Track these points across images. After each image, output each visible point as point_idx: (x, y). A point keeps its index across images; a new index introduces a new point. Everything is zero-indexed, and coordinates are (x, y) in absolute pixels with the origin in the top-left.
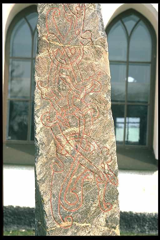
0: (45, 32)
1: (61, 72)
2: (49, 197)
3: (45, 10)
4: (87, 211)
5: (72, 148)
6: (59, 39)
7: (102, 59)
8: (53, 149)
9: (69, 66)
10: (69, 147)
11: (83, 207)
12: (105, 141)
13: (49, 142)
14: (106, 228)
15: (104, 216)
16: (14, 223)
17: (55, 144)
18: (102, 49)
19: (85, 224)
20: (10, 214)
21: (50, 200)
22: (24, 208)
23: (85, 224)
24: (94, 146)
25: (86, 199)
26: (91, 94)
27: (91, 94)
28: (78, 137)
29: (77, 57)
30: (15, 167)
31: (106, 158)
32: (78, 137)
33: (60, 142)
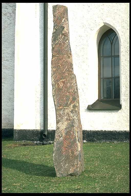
0: (54, 52)
1: (58, 64)
2: (56, 100)
3: (54, 46)
4: (67, 103)
5: (62, 86)
6: (58, 54)
7: (70, 59)
8: (57, 86)
9: (61, 62)
10: (61, 85)
11: (66, 102)
12: (72, 83)
13: (56, 84)
14: (73, 108)
15: (72, 105)
16: (103, 139)
17: (58, 85)
18: (70, 56)
19: (67, 107)
20: (101, 134)
21: (56, 101)
22: (108, 131)
23: (67, 107)
24: (69, 85)
25: (67, 100)
26: (67, 69)
27: (67, 69)
28: (64, 82)
29: (63, 59)
30: (105, 111)
31: (72, 88)
32: (64, 82)
33: (58, 84)
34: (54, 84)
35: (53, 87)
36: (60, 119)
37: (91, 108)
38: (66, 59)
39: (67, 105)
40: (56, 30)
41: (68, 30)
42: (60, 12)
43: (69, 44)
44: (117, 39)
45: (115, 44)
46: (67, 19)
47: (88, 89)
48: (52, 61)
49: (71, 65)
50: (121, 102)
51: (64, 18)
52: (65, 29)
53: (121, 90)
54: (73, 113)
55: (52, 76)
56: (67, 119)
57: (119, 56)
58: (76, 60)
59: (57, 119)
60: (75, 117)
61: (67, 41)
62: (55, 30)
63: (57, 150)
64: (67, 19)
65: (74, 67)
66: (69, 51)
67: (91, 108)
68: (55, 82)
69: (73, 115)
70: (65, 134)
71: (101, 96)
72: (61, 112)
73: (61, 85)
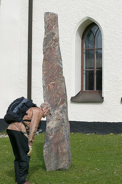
4: (57, 104)
12: (61, 86)
24: (59, 87)
32: (54, 85)
34: (45, 86)
36: (50, 118)
37: (74, 100)
38: (57, 63)
41: (58, 36)
42: (51, 19)
43: (59, 49)
44: (99, 32)
45: (97, 38)
50: (103, 94)
51: (55, 25)
52: (56, 36)
54: (63, 113)
55: (43, 78)
57: (102, 49)
58: (66, 73)
59: (47, 119)
61: (58, 47)
66: (59, 56)
67: (74, 100)
68: (46, 84)
71: (83, 69)
73: (52, 87)
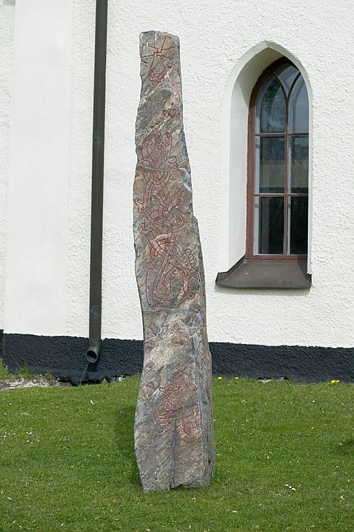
4: (175, 299)
24: (180, 247)
32: (166, 241)
33: (152, 245)
34: (141, 245)
35: (136, 255)
37: (226, 281)
39: (173, 304)
40: (149, 99)
41: (180, 100)
42: (159, 50)
45: (295, 102)
46: (179, 71)
47: (222, 226)
48: (135, 182)
49: (189, 196)
50: (310, 267)
52: (173, 100)
53: (312, 209)
54: (191, 325)
55: (135, 222)
56: (174, 342)
57: (308, 134)
60: (195, 335)
61: (178, 131)
62: (145, 101)
63: (147, 422)
64: (178, 71)
65: (195, 201)
67: (226, 281)
68: (143, 239)
69: (190, 330)
70: (168, 380)
72: (159, 322)
73: (160, 248)
